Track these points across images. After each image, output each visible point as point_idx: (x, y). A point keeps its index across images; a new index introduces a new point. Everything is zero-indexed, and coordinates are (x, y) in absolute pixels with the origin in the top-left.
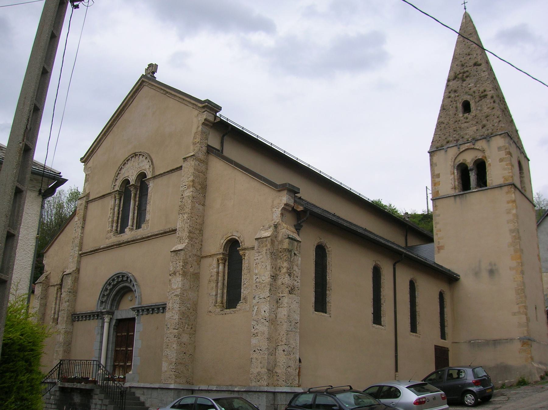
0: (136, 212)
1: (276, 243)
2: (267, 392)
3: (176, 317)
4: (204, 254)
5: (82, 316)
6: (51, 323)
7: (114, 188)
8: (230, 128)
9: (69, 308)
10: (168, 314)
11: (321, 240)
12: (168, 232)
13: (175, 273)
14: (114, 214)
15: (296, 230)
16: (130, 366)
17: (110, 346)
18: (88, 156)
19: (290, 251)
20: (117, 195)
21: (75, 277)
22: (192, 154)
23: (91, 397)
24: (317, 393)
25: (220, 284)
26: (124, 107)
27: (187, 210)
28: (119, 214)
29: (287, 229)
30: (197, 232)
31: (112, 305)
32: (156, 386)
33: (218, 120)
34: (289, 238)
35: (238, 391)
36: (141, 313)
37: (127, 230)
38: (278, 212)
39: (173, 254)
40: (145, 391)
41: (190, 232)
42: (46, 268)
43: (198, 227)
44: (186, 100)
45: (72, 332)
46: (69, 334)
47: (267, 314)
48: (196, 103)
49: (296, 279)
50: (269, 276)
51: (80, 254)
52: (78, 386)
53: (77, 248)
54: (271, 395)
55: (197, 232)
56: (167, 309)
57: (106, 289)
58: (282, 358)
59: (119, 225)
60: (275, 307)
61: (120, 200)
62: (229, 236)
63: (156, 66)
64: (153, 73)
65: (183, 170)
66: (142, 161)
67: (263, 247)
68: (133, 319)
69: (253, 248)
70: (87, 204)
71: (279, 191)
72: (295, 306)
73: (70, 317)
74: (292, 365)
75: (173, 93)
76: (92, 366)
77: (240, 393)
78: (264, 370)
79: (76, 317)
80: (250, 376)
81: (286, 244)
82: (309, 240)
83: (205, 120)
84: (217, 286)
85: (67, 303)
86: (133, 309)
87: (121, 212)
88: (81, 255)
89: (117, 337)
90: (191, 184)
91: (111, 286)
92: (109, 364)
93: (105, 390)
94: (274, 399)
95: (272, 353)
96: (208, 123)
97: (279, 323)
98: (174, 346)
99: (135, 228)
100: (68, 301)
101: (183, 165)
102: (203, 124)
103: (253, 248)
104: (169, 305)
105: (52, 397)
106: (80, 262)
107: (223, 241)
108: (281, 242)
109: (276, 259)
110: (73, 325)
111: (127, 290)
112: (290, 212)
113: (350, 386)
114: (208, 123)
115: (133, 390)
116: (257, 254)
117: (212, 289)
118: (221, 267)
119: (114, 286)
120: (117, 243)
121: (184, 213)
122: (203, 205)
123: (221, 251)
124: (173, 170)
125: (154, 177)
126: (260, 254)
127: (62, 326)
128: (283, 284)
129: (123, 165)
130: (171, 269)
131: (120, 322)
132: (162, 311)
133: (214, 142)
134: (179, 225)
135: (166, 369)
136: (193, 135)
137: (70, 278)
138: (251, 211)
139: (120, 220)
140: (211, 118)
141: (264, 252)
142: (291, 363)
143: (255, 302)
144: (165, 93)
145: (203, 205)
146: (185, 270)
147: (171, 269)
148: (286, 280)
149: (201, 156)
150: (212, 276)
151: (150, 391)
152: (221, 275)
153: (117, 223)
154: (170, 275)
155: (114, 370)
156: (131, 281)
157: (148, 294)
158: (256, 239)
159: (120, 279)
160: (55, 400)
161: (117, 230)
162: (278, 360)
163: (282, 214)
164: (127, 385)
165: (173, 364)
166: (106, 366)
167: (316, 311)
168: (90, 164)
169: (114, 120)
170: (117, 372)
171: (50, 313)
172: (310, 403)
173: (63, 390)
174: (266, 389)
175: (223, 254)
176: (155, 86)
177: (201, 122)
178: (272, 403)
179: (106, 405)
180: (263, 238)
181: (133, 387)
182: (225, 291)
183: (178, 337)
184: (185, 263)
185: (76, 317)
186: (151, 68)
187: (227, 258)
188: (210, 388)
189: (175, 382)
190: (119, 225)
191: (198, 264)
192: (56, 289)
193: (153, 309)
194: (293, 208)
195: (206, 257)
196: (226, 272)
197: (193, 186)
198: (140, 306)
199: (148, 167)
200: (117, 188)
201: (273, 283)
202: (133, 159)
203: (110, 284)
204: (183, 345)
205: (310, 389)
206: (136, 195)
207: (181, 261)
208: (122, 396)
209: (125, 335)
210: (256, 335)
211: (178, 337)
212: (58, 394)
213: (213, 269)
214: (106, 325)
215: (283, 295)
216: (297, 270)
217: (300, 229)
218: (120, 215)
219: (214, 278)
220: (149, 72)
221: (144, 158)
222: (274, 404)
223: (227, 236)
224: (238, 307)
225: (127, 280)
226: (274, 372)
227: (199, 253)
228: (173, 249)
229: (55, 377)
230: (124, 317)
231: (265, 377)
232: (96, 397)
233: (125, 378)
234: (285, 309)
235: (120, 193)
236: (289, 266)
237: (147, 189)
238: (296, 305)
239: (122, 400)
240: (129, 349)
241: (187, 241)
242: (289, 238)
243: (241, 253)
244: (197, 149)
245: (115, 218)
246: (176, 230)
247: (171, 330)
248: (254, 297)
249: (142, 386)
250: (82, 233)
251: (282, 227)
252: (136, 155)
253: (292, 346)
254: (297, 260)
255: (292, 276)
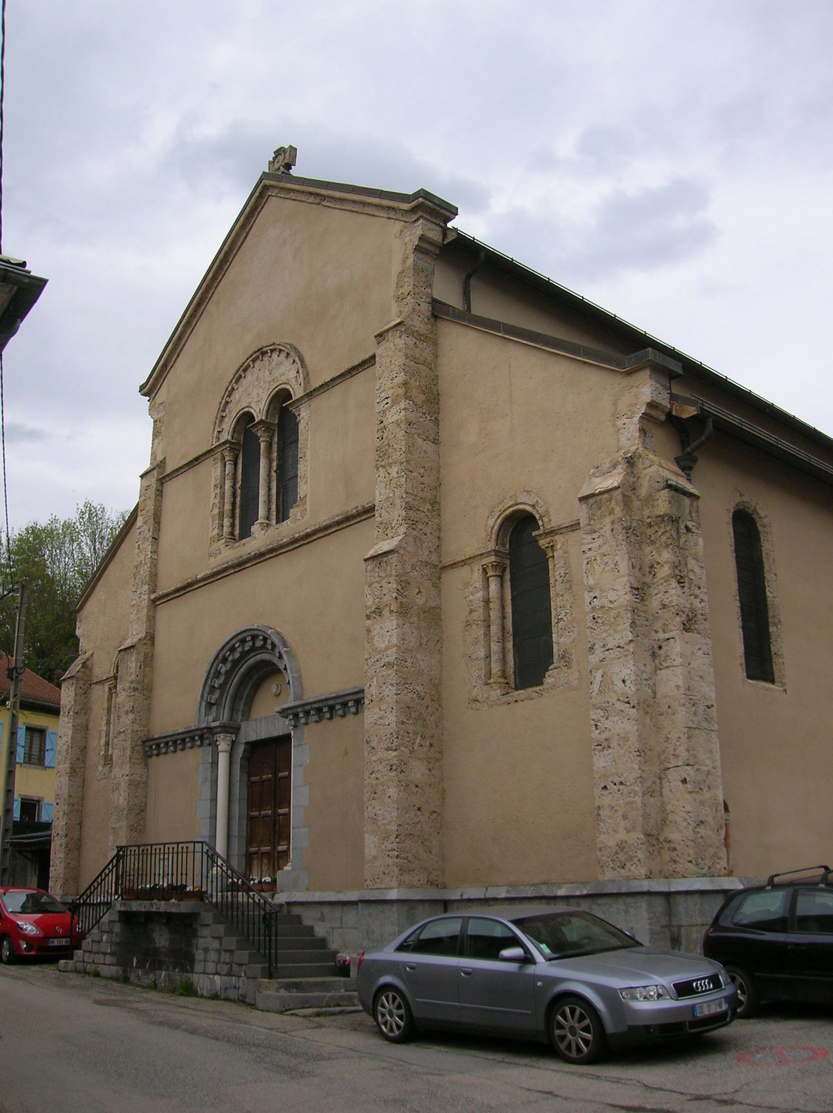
0: (274, 485)
1: (637, 504)
2: (649, 893)
3: (391, 718)
4: (447, 560)
5: (167, 744)
6: (100, 768)
7: (218, 439)
8: (482, 255)
9: (136, 727)
10: (370, 715)
11: (746, 498)
12: (353, 517)
13: (378, 611)
14: (223, 498)
15: (683, 469)
16: (286, 853)
17: (236, 807)
18: (157, 379)
19: (674, 521)
20: (226, 453)
21: (146, 654)
22: (398, 321)
23: (195, 934)
24: (796, 888)
25: (495, 629)
26: (227, 254)
27: (396, 456)
28: (234, 495)
29: (659, 467)
30: (427, 505)
31: (233, 709)
32: (353, 895)
33: (451, 237)
34: (669, 487)
35: (567, 898)
36: (303, 721)
37: (255, 528)
38: (632, 426)
39: (371, 565)
40: (326, 910)
41: (408, 508)
42: (83, 644)
43: (427, 494)
44: (370, 204)
45: (146, 783)
46: (140, 787)
47: (630, 689)
48: (395, 204)
49: (697, 592)
50: (628, 589)
51: (154, 601)
52: (161, 906)
53: (146, 587)
54: (660, 903)
55: (427, 505)
56: (367, 702)
57: (218, 674)
58: (680, 802)
59: (237, 521)
60: (649, 669)
61: (236, 464)
62: (507, 506)
63: (293, 150)
64: (288, 166)
65: (377, 364)
66: (281, 363)
67: (602, 517)
68: (285, 739)
69: (575, 527)
70: (162, 484)
71: (629, 374)
72: (700, 662)
73: (139, 748)
74: (710, 819)
75: (338, 194)
76: (190, 856)
77: (572, 901)
78: (636, 837)
79: (152, 747)
80: (599, 854)
81: (663, 504)
82: (718, 494)
83: (422, 238)
84: (487, 634)
85: (131, 716)
86: (284, 713)
87: (239, 491)
88: (155, 603)
89: (251, 785)
90: (401, 391)
91: (229, 665)
92: (235, 850)
93: (226, 913)
94: (670, 913)
95: (654, 789)
96: (429, 247)
97: (663, 709)
98: (392, 791)
99: (274, 522)
100: (132, 711)
101: (378, 352)
102: (418, 249)
103: (575, 527)
104: (372, 692)
105: (105, 938)
106: (154, 617)
107: (494, 522)
108: (649, 500)
109: (640, 543)
110: (147, 765)
111: (268, 671)
112: (661, 424)
113: (826, 868)
114: (429, 247)
115: (296, 911)
116: (589, 538)
117: (474, 640)
118: (494, 586)
119: (236, 663)
120: (235, 561)
121: (390, 465)
122: (436, 441)
123: (492, 546)
124: (354, 368)
125: (310, 395)
126: (595, 536)
127: (122, 772)
128: (664, 606)
129: (236, 382)
130: (369, 603)
131: (255, 748)
132: (353, 710)
133: (447, 289)
134: (379, 495)
135: (374, 853)
136: (394, 279)
137: (134, 658)
138: (552, 440)
139: (238, 511)
140: (435, 235)
141: (608, 528)
142: (708, 814)
143: (593, 659)
144: (318, 200)
145: (436, 441)
146: (404, 600)
147: (369, 603)
148: (674, 594)
149: (419, 324)
150: (471, 611)
151: (338, 911)
152: (495, 605)
153: (233, 516)
154: (368, 617)
155: (249, 865)
156: (274, 645)
157: (317, 673)
158: (583, 499)
159: (247, 647)
160: (112, 943)
161: (232, 533)
162: (669, 808)
163: (643, 431)
164: (281, 898)
165: (392, 838)
166: (228, 856)
167: (750, 676)
168: (162, 395)
169: (208, 288)
170: (255, 869)
171: (97, 743)
172: (779, 915)
173: (127, 918)
174: (646, 886)
175: (497, 553)
176: (293, 190)
177: (411, 247)
178: (664, 922)
179: (231, 951)
180: (601, 493)
181: (295, 903)
182: (510, 645)
183: (399, 768)
184: (404, 584)
185: (152, 747)
186: (281, 158)
187: (508, 562)
188: (491, 893)
189: (401, 884)
190: (237, 521)
191: (436, 586)
192: (107, 689)
193: (332, 708)
194: (669, 415)
195: (454, 565)
196: (508, 596)
197: (407, 397)
198: (299, 703)
199: (293, 374)
200: (226, 436)
201: (639, 606)
202: (258, 363)
203: (224, 660)
204: (414, 789)
205: (772, 878)
206: (270, 445)
207: (392, 579)
208: (268, 926)
209: (269, 780)
210: (603, 745)
211: (399, 768)
212: (117, 928)
213: (474, 594)
214: (223, 759)
215: (667, 636)
216: (697, 569)
217: (691, 468)
218: (238, 499)
219: (479, 614)
220: (277, 166)
221: (283, 355)
222: (669, 926)
223: (501, 508)
224: (548, 680)
225: (264, 647)
226: (662, 839)
227: (434, 559)
228: (372, 552)
229: (109, 892)
230: (263, 735)
231: (641, 855)
232: (205, 932)
233: (274, 881)
234: (679, 670)
235: (232, 446)
236: (676, 560)
237: (297, 425)
238: (701, 660)
239: (270, 936)
240: (281, 811)
241: (402, 530)
242: (669, 487)
243: (543, 543)
244: (406, 310)
245: (228, 507)
246: (372, 509)
247: (382, 754)
248: (591, 648)
249: (316, 899)
250: (155, 552)
251: (647, 463)
252: (264, 354)
253: (705, 768)
254: (696, 545)
255: (686, 585)
